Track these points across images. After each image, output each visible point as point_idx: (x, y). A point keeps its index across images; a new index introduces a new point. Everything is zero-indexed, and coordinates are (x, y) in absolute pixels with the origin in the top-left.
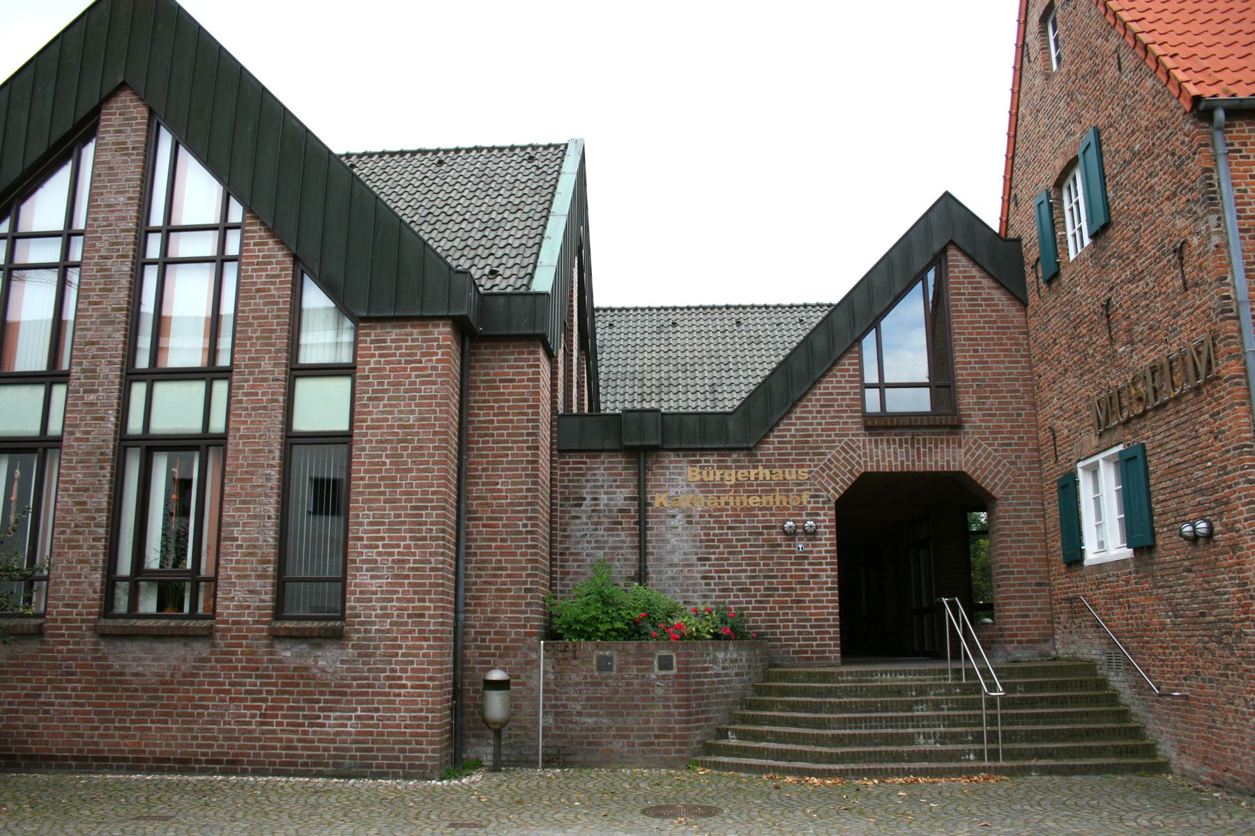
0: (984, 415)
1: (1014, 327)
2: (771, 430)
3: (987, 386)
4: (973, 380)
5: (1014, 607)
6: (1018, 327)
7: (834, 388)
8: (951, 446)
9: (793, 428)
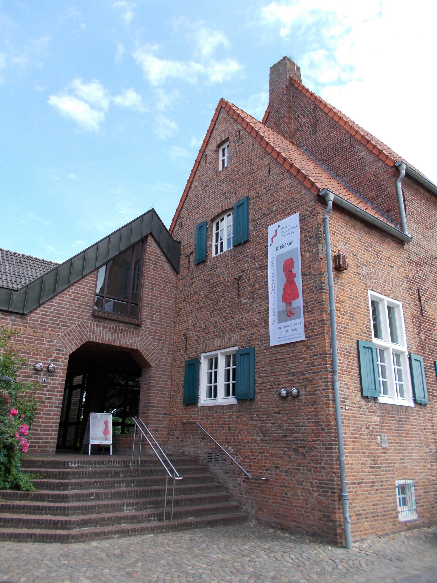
0: (152, 323)
1: (171, 283)
2: (39, 306)
3: (155, 308)
4: (149, 304)
5: (152, 425)
6: (173, 283)
7: (80, 291)
8: (134, 335)
9: (53, 308)
